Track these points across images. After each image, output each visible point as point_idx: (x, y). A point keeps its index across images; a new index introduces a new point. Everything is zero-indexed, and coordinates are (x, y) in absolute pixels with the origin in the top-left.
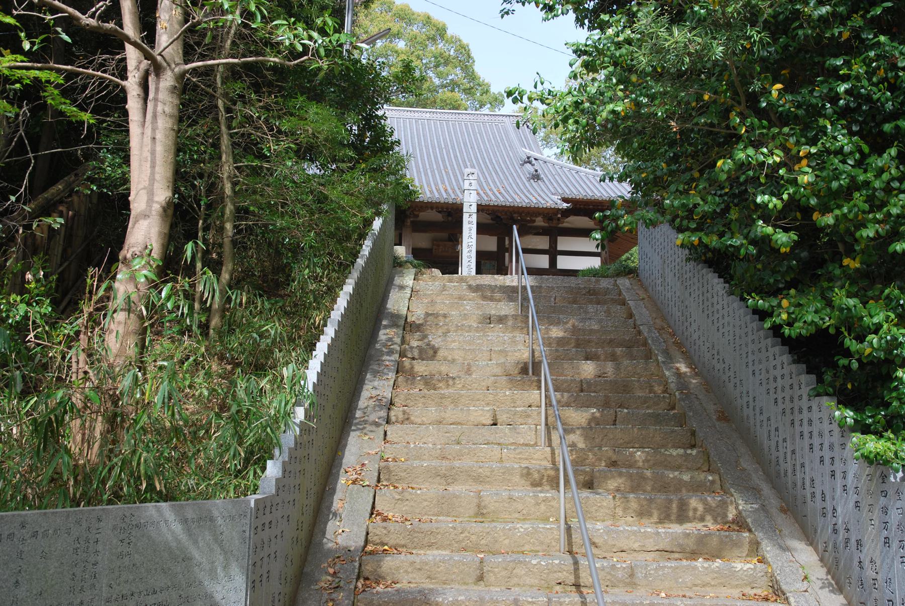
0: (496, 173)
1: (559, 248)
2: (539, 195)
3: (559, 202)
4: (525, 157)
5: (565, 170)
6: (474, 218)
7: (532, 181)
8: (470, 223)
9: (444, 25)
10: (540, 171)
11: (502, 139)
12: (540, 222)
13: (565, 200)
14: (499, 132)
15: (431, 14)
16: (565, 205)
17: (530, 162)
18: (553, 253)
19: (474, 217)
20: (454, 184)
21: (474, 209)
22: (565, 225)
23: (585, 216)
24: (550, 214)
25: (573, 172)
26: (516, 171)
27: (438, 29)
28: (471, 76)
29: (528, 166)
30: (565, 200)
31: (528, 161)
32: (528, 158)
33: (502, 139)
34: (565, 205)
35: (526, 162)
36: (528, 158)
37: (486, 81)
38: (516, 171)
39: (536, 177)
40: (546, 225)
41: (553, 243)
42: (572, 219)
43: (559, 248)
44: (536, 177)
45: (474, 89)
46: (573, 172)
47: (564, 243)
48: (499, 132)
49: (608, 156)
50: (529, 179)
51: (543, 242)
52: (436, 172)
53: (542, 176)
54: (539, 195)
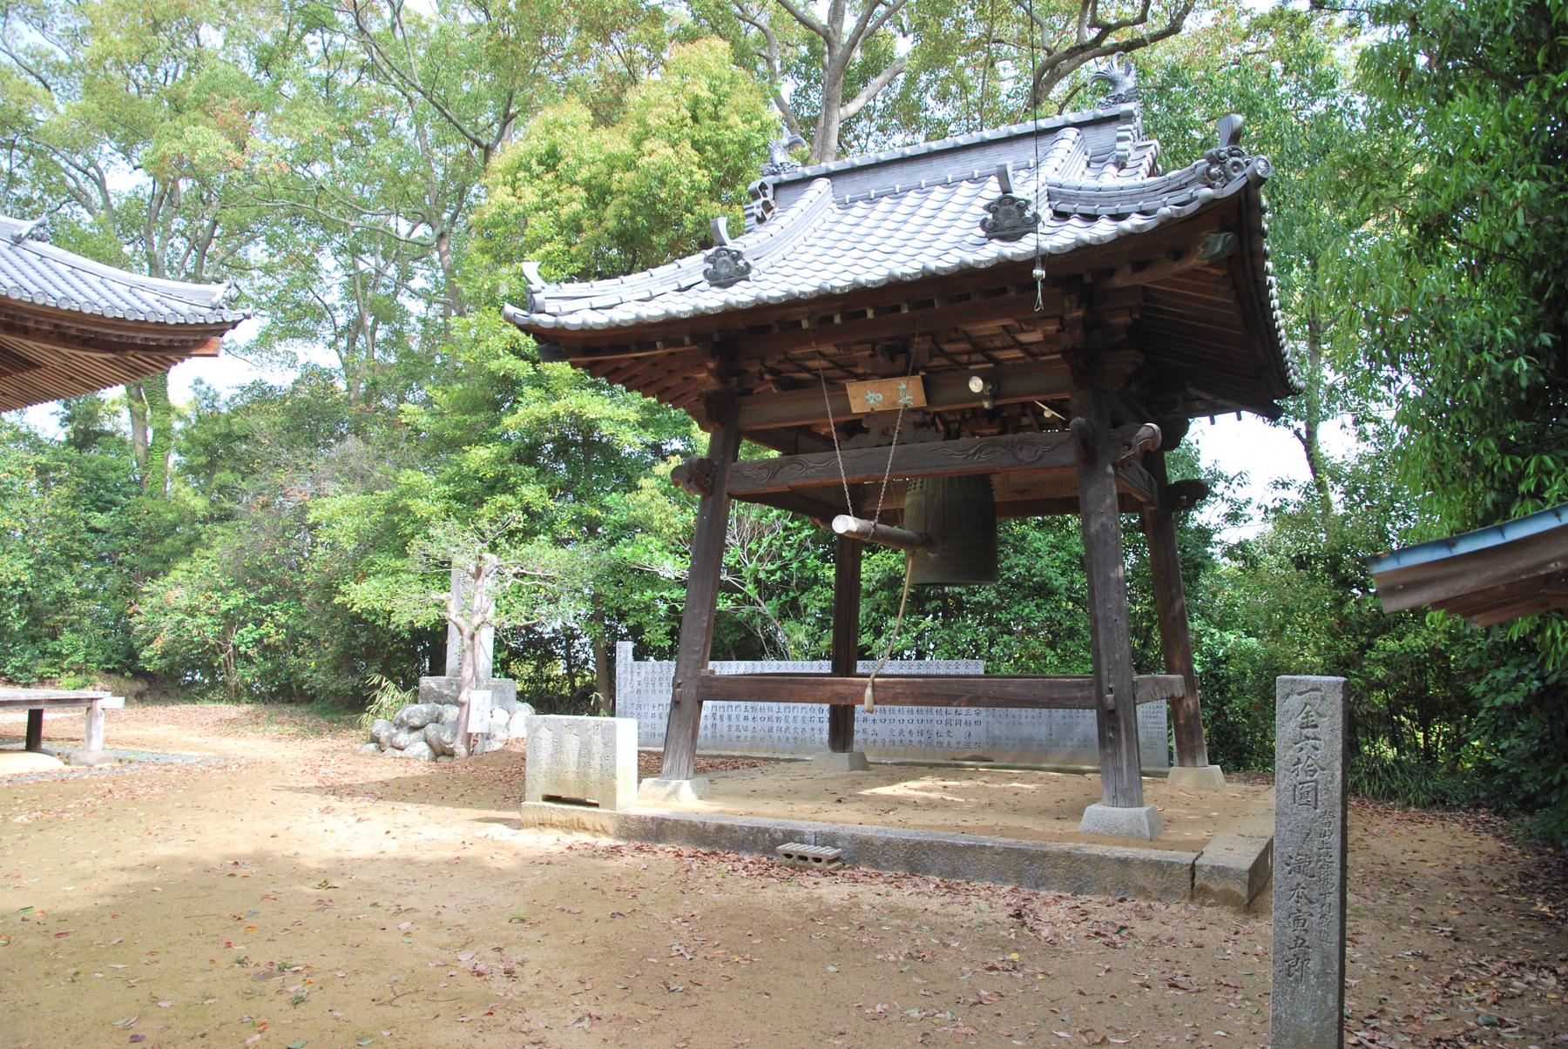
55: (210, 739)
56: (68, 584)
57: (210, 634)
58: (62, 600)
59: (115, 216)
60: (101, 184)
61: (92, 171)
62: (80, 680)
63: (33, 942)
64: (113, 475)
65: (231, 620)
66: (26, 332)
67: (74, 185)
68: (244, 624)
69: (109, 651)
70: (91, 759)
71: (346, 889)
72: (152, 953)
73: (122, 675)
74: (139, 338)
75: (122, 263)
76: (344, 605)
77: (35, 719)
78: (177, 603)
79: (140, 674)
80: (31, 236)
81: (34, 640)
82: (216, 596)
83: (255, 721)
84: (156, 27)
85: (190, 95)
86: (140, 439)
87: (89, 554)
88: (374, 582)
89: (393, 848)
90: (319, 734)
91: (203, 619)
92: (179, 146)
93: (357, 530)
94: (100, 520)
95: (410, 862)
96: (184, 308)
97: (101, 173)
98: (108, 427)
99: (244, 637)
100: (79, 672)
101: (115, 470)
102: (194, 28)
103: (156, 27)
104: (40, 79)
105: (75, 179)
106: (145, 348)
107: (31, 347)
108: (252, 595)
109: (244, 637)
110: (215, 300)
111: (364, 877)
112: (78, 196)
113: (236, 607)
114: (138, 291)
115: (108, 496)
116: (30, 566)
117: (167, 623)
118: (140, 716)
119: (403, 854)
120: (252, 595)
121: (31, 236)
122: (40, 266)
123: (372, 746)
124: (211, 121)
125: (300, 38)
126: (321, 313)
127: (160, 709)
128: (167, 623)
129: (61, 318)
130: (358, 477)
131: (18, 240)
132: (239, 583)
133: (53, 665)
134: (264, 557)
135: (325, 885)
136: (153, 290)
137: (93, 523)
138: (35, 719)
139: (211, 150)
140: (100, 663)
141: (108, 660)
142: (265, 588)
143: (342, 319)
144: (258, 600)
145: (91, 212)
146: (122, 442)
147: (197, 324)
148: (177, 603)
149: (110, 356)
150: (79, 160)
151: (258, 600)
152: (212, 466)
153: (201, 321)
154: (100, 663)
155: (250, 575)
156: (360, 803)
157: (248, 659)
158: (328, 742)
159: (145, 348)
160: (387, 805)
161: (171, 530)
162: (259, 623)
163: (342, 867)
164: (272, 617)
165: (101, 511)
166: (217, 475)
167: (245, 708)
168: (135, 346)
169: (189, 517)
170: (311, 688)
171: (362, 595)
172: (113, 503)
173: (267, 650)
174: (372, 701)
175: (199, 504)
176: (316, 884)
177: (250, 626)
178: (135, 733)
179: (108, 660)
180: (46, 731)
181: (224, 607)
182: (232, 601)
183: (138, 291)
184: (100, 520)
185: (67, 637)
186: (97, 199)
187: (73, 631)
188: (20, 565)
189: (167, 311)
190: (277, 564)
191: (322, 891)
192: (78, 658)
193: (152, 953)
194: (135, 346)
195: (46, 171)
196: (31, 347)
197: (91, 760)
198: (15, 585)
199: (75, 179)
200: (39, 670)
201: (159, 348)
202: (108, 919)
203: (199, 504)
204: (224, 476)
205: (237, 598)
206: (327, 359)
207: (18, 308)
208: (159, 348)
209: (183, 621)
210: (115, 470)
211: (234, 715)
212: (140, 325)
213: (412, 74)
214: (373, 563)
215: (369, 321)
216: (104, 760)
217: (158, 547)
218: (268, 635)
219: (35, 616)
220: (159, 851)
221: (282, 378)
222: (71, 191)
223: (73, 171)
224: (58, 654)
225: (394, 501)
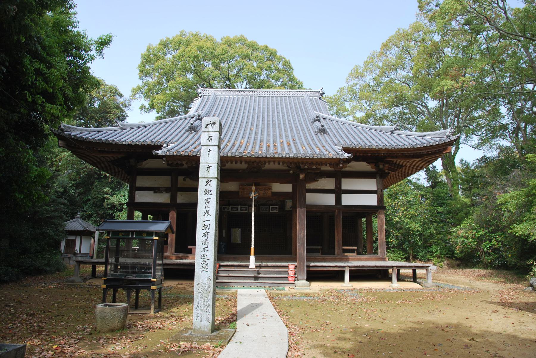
0: (291, 129)
1: (343, 188)
2: (324, 147)
3: (341, 152)
4: (315, 117)
5: (346, 125)
6: (214, 185)
7: (319, 134)
8: (207, 192)
9: (275, 50)
10: (326, 127)
11: (300, 107)
12: (328, 168)
13: (346, 150)
14: (299, 102)
15: (268, 46)
16: (346, 155)
17: (319, 121)
18: (338, 192)
19: (214, 183)
20: (310, 140)
21: (214, 172)
22: (347, 169)
23: (363, 161)
24: (335, 162)
25: (353, 127)
26: (308, 128)
27: (272, 53)
28: (292, 79)
29: (317, 123)
30: (346, 150)
31: (318, 119)
32: (317, 117)
33: (300, 107)
34: (346, 155)
35: (315, 121)
36: (317, 117)
37: (301, 81)
38: (308, 128)
39: (322, 131)
40: (332, 169)
41: (338, 184)
42: (353, 164)
43: (343, 188)
44: (322, 131)
45: (294, 84)
46: (353, 127)
47: (347, 184)
48: (299, 102)
49: (371, 122)
50: (317, 133)
51: (329, 183)
52: (308, 135)
53: (328, 130)
54: (324, 147)
55: (472, 282)
56: (432, 230)
57: (474, 244)
58: (432, 235)
59: (433, 115)
60: (426, 107)
61: (423, 104)
62: (439, 260)
63: (375, 340)
64: (442, 195)
65: (480, 240)
66: (397, 157)
67: (419, 110)
68: (485, 241)
69: (447, 251)
70: (428, 285)
71: (480, 343)
72: (401, 351)
73: (452, 259)
74: (426, 152)
75: (436, 129)
76: (512, 233)
77: (414, 272)
78: (463, 234)
79: (457, 259)
80: (395, 130)
81: (426, 248)
82: (474, 232)
83: (490, 276)
84: (431, 55)
85: (441, 71)
86: (449, 182)
87: (438, 220)
88: (525, 224)
89: (511, 330)
90: (512, 282)
91: (470, 240)
92: (439, 88)
93: (516, 205)
94: (440, 209)
95: (515, 337)
96: (438, 139)
97: (426, 104)
98: (439, 180)
99: (486, 245)
100: (439, 258)
101: (443, 193)
102: (443, 51)
103: (431, 55)
104: (406, 84)
105: (420, 108)
106: (428, 154)
107: (400, 161)
108: (487, 231)
109: (486, 245)
110: (447, 134)
111: (490, 339)
112: (421, 113)
113: (481, 235)
114: (424, 138)
115: (442, 202)
116: (421, 225)
117: (459, 241)
118: (454, 272)
119: (514, 333)
120: (487, 231)
121: (395, 130)
122: (383, 135)
123: (530, 288)
124: (448, 77)
125: (475, 38)
126: (504, 127)
127: (460, 270)
128: (459, 241)
129: (403, 151)
130: (518, 185)
131: (392, 132)
132: (481, 227)
133: (431, 255)
134: (489, 217)
135: (473, 339)
136: (428, 136)
137: (439, 210)
138: (414, 272)
139: (449, 86)
140: (445, 255)
141: (447, 254)
142: (491, 228)
143: (511, 128)
144: (489, 232)
145: (425, 116)
146: (445, 184)
147: (443, 143)
148: (463, 234)
149: (420, 159)
150: (420, 103)
151: (489, 232)
152: (470, 189)
153: (444, 142)
154: (445, 255)
155: (485, 224)
156: (512, 310)
157: (489, 254)
158: (516, 285)
159: (428, 154)
160: (521, 313)
161: (461, 210)
162: (490, 241)
163: (484, 334)
164: (495, 238)
165: (441, 206)
166: (472, 190)
167: (489, 271)
168: (426, 155)
169: (465, 206)
170: (510, 264)
171: (520, 229)
172: (444, 204)
173: (496, 250)
174: (531, 271)
175: (467, 201)
176: (469, 338)
177: (488, 242)
178: (450, 278)
179: (447, 254)
180: (418, 275)
181: (477, 236)
182: (480, 233)
183: (424, 138)
184: (440, 209)
185: (434, 246)
186: (426, 112)
187: (436, 245)
188: (418, 225)
189: (432, 141)
190: (494, 219)
191: (471, 342)
192: (438, 253)
193: (401, 351)
194: (426, 155)
195: (413, 110)
196: (400, 161)
197: (429, 286)
198: (418, 231)
199: (420, 108)
200: (428, 257)
201: (432, 154)
202: (397, 337)
203: (467, 201)
204: (474, 190)
205: (481, 232)
206: (505, 143)
207: (392, 151)
208: (432, 154)
209: (464, 241)
210: (443, 193)
211: (484, 273)
212: (425, 148)
213: (516, 33)
214: (524, 217)
215: (523, 125)
216: (432, 286)
217: (457, 216)
218: (494, 245)
219: (425, 241)
220: (428, 318)
221: (493, 153)
222: (419, 112)
223: (419, 106)
224: (432, 252)
225: (530, 192)
